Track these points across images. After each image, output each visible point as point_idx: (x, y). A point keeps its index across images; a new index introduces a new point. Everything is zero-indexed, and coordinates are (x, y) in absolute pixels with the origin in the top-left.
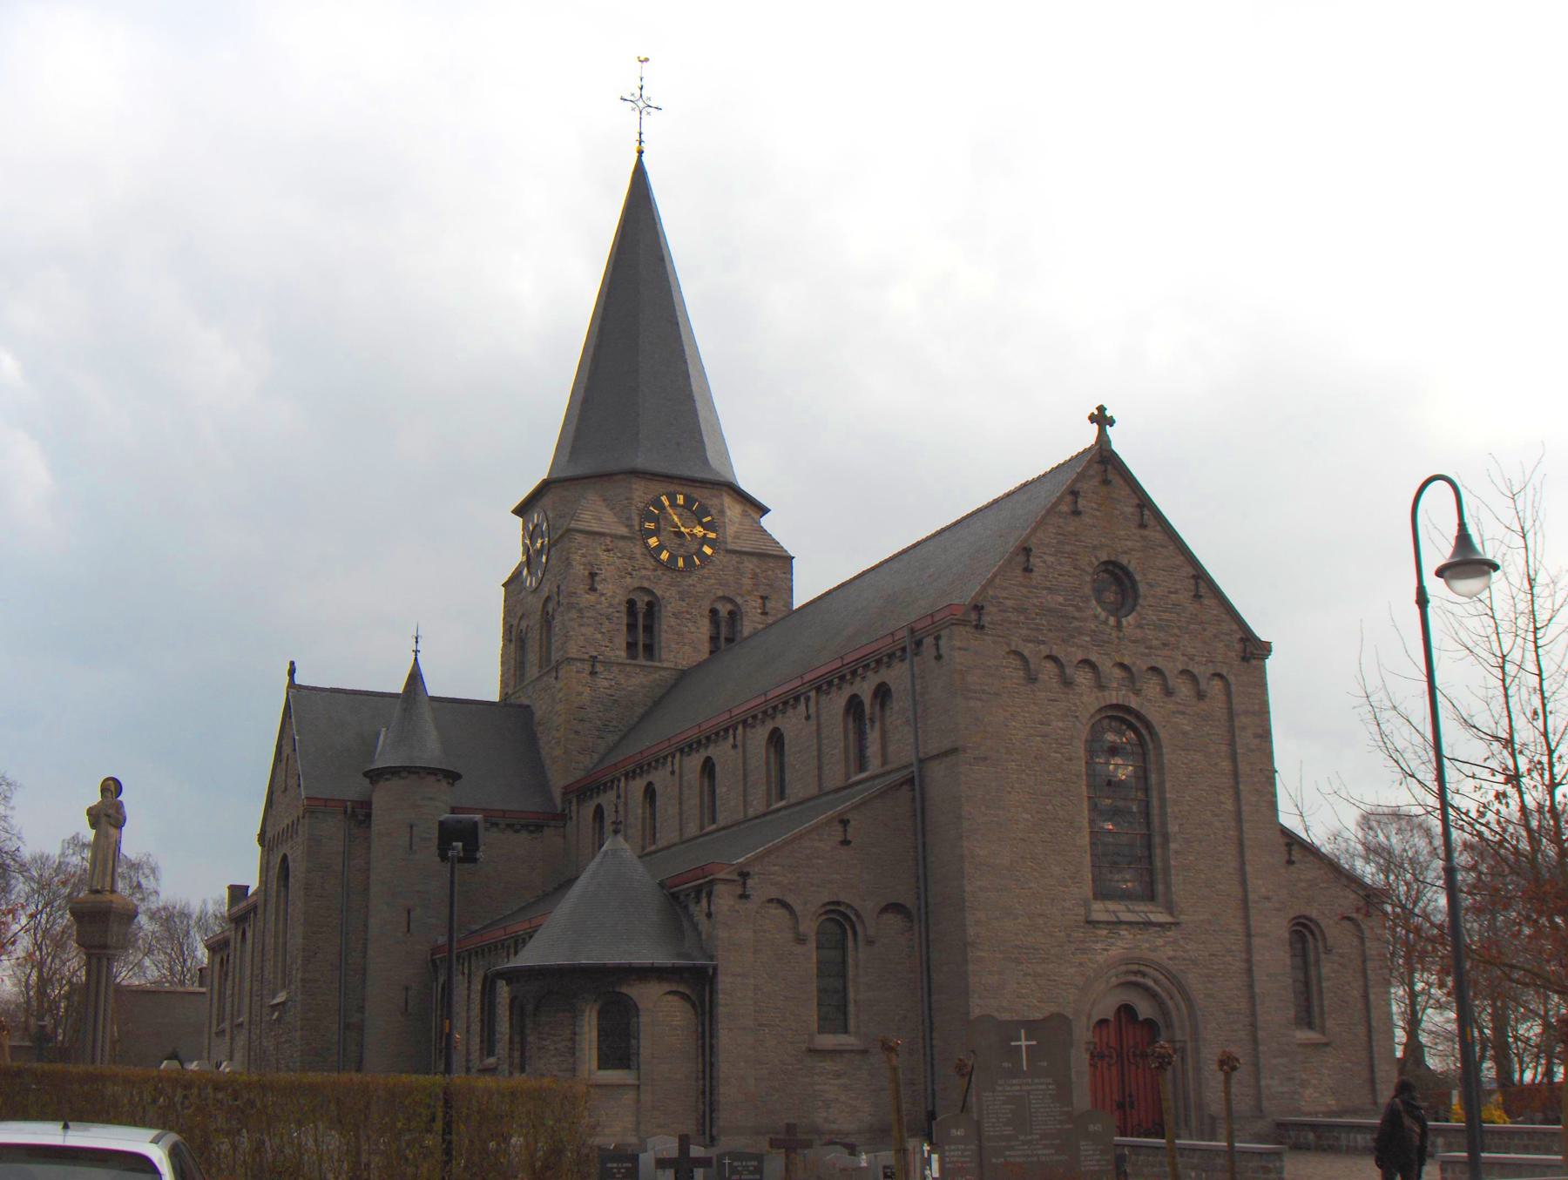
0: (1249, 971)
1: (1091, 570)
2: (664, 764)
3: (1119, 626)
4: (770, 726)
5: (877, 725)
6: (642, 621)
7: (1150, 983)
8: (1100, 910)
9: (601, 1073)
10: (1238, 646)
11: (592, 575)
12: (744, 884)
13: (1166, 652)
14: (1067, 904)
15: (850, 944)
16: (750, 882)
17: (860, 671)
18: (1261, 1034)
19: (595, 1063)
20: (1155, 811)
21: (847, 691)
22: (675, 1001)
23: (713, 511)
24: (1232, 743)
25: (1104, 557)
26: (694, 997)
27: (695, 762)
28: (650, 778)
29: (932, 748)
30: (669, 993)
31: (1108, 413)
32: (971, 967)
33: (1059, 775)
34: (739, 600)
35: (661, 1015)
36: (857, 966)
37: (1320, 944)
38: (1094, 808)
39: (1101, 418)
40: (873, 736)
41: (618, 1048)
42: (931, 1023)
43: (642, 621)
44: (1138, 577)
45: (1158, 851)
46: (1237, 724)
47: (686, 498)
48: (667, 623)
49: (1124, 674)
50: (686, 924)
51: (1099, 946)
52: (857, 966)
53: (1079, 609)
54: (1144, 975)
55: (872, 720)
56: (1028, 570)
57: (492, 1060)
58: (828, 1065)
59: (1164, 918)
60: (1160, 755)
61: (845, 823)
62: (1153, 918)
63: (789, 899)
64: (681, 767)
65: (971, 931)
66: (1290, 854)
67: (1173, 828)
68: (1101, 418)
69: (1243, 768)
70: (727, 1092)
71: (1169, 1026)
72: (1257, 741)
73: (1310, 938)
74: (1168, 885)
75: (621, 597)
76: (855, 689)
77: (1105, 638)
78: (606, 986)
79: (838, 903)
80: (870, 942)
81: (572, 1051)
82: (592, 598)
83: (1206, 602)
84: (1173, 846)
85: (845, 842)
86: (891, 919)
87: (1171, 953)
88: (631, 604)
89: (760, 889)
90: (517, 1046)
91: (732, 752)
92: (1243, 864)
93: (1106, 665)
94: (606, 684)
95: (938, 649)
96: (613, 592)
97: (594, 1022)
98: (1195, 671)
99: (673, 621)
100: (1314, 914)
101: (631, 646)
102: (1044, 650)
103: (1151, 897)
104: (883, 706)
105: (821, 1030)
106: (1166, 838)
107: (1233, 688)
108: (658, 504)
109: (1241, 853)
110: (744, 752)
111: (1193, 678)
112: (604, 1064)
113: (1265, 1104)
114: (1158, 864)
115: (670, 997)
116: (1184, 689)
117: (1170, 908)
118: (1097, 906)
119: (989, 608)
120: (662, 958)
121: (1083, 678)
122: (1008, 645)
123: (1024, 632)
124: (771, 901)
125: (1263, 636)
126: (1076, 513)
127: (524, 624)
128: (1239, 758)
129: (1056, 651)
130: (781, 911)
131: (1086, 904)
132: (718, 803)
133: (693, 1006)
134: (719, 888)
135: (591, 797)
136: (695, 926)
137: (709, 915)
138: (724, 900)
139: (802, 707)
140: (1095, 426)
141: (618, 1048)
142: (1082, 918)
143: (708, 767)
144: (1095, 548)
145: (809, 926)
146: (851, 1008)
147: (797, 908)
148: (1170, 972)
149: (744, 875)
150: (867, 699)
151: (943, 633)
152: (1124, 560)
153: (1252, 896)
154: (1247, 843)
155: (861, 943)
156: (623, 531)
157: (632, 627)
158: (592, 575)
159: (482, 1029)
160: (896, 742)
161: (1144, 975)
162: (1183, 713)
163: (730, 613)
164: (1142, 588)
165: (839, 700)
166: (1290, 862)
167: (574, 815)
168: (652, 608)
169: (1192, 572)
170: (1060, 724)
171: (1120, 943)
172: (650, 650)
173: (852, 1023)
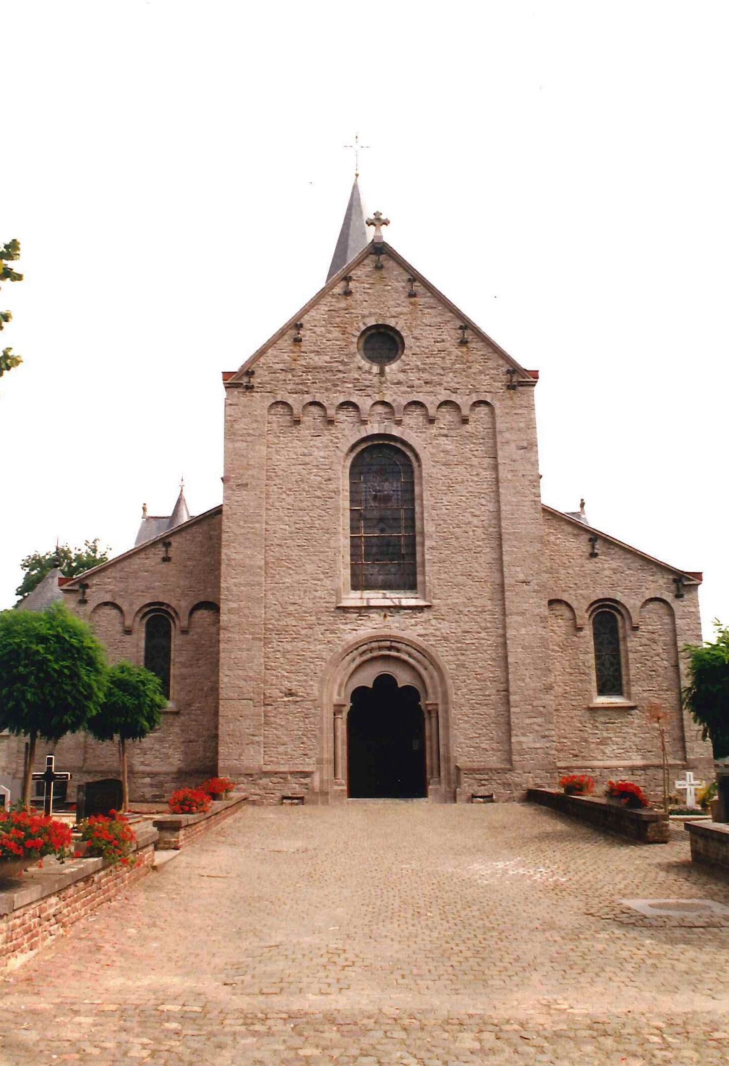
3: (382, 373)
7: (405, 657)
8: (353, 599)
12: (84, 593)
13: (428, 388)
18: (512, 698)
31: (383, 217)
32: (222, 646)
37: (627, 623)
44: (403, 334)
49: (387, 410)
56: (297, 341)
59: (421, 603)
61: (167, 545)
62: (404, 603)
63: (118, 602)
66: (593, 547)
67: (429, 528)
69: (503, 474)
73: (619, 617)
77: (367, 383)
85: (166, 559)
87: (423, 632)
98: (458, 401)
100: (618, 597)
102: (308, 398)
103: (411, 586)
113: (515, 758)
119: (259, 372)
123: (289, 387)
125: (526, 363)
130: (115, 612)
147: (125, 608)
152: (392, 323)
154: (504, 537)
162: (446, 436)
169: (459, 323)
171: (369, 624)
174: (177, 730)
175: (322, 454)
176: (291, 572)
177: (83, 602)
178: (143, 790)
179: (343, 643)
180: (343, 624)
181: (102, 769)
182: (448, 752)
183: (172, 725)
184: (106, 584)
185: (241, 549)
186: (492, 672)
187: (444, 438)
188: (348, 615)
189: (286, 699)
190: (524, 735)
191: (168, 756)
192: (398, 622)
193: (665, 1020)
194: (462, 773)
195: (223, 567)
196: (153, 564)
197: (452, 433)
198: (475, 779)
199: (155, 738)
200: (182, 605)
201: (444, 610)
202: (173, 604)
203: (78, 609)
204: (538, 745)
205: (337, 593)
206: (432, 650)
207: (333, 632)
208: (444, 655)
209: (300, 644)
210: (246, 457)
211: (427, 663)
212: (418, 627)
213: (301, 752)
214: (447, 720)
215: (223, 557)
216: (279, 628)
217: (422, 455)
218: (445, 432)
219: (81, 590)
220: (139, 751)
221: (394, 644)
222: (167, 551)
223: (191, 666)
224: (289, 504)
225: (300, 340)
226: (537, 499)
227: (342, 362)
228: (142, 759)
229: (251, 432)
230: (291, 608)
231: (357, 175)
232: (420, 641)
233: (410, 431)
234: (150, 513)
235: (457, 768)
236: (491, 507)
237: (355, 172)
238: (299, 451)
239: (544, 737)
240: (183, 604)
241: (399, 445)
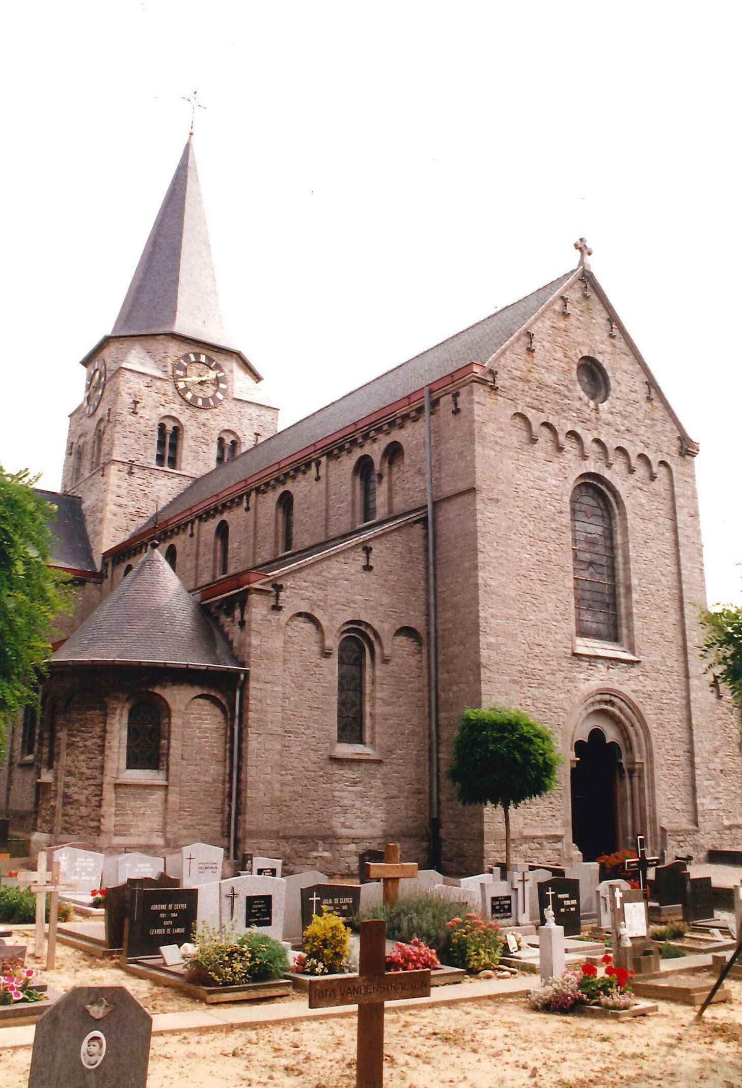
0: (688, 706)
1: (577, 361)
2: (184, 530)
4: (280, 490)
5: (385, 479)
6: (169, 443)
9: (130, 771)
10: (678, 443)
11: (136, 403)
12: (277, 597)
14: (558, 637)
15: (368, 660)
16: (282, 594)
17: (372, 434)
18: (697, 760)
19: (123, 762)
20: (620, 566)
21: (358, 453)
22: (205, 704)
23: (226, 370)
24: (674, 519)
25: (585, 354)
26: (224, 702)
27: (211, 525)
28: (172, 542)
29: (448, 489)
33: (553, 525)
34: (239, 434)
35: (193, 722)
36: (373, 682)
39: (581, 247)
41: (148, 749)
42: (438, 736)
43: (169, 443)
44: (609, 374)
45: (622, 600)
46: (677, 504)
47: (207, 358)
48: (187, 445)
49: (600, 450)
50: (217, 634)
51: (582, 676)
52: (373, 682)
53: (569, 390)
54: (612, 704)
55: (380, 476)
56: (530, 351)
57: (30, 758)
58: (348, 773)
60: (624, 519)
61: (368, 550)
63: (318, 614)
64: (199, 530)
65: (484, 653)
67: (634, 581)
68: (581, 247)
69: (682, 539)
70: (255, 794)
71: (630, 749)
74: (630, 630)
75: (155, 421)
76: (367, 450)
78: (139, 689)
79: (359, 622)
80: (386, 661)
81: (102, 749)
82: (132, 418)
83: (655, 404)
84: (635, 596)
85: (368, 568)
86: (402, 640)
87: (635, 688)
88: (162, 427)
89: (292, 601)
90: (46, 742)
91: (245, 514)
92: (683, 616)
93: (587, 438)
94: (140, 481)
95: (456, 404)
96: (151, 416)
97: (125, 720)
99: (192, 443)
101: (160, 459)
103: (615, 638)
104: (391, 463)
105: (341, 740)
106: (629, 589)
107: (675, 475)
108: (186, 358)
109: (681, 608)
110: (256, 513)
111: (648, 463)
112: (133, 762)
113: (700, 819)
114: (623, 611)
115: (201, 701)
116: (641, 471)
117: (632, 649)
118: (579, 641)
120: (197, 661)
121: (569, 446)
122: (516, 407)
123: (528, 400)
124: (300, 614)
126: (566, 315)
127: (82, 441)
128: (679, 531)
129: (552, 420)
130: (309, 627)
132: (230, 556)
133: (223, 710)
134: (254, 598)
135: (123, 561)
136: (225, 636)
137: (242, 624)
138: (258, 609)
139: (313, 471)
140: (578, 252)
141: (148, 749)
142: (570, 651)
143: (223, 531)
144: (579, 344)
145: (333, 642)
146: (368, 722)
147: (324, 623)
148: (632, 703)
149: (279, 588)
150: (377, 459)
151: (461, 391)
152: (600, 358)
153: (689, 644)
155: (378, 660)
156: (159, 374)
157: (161, 444)
158: (136, 403)
159: (25, 731)
160: (407, 487)
161: (612, 704)
163: (232, 442)
164: (613, 384)
165: (348, 462)
167: (109, 574)
168: (177, 432)
170: (554, 482)
172: (173, 462)
173: (367, 734)
174: (378, 783)
175: (554, 482)
176: (536, 609)
177: (277, 608)
178: (348, 860)
179: (579, 694)
180: (577, 672)
181: (300, 833)
182: (654, 813)
183: (374, 777)
184: (301, 589)
185: (496, 575)
186: (680, 734)
187: (639, 491)
188: (581, 663)
190: (704, 797)
191: (369, 816)
192: (619, 676)
194: (668, 833)
195: (481, 593)
196: (353, 571)
198: (676, 841)
199: (356, 793)
200: (385, 628)
201: (648, 667)
202: (376, 625)
203: (269, 617)
204: (713, 807)
206: (640, 706)
207: (571, 680)
208: (649, 713)
209: (546, 691)
210: (495, 468)
211: (635, 720)
212: (632, 682)
213: (550, 813)
214: (652, 781)
215: (480, 581)
216: (529, 671)
217: (627, 503)
218: (640, 485)
219: (274, 593)
220: (339, 809)
221: (613, 698)
222: (368, 558)
223: (392, 704)
224: (530, 531)
225: (533, 351)
227: (566, 386)
228: (342, 820)
229: (498, 440)
230: (537, 650)
231: (191, 134)
232: (633, 697)
233: (615, 476)
235: (663, 829)
236: (673, 569)
237: (190, 130)
238: (537, 473)
239: (717, 798)
240: (386, 626)
241: (603, 488)
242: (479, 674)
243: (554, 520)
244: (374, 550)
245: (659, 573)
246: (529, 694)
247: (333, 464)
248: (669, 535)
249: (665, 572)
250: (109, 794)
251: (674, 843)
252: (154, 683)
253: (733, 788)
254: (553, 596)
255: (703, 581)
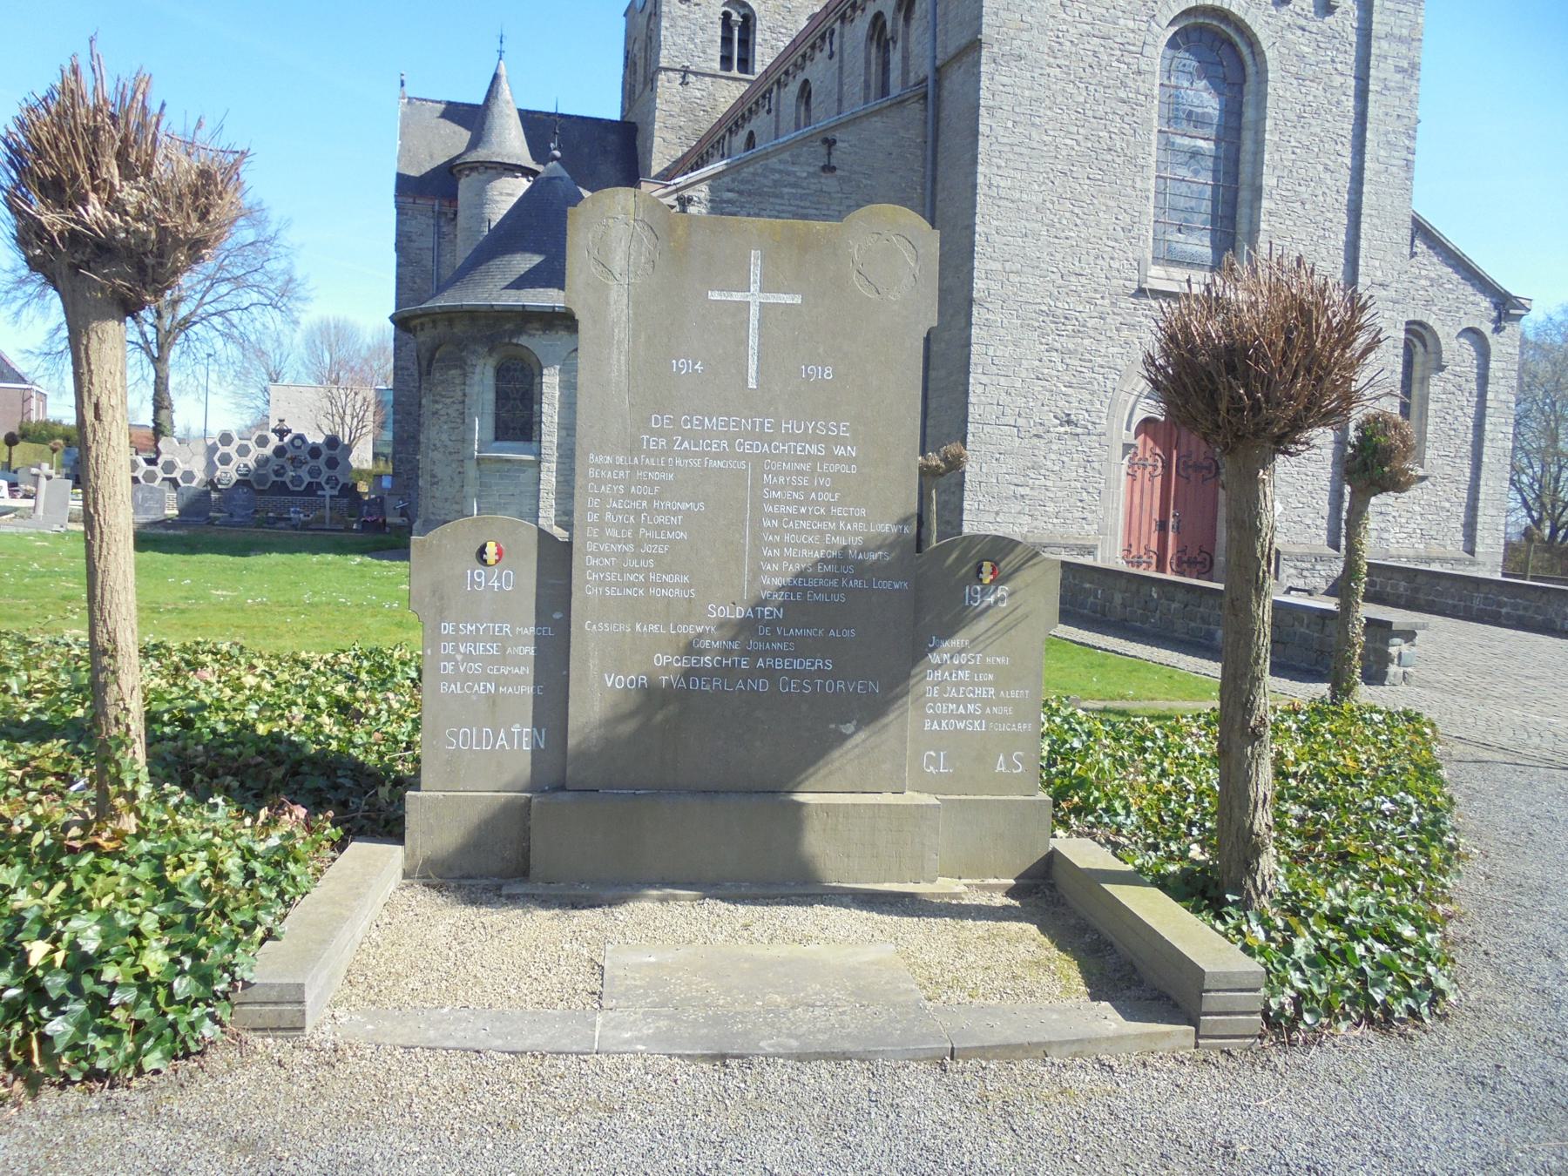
5: (899, 45)
30: (1276, 578)
38: (1168, 146)
40: (895, 57)
61: (830, 143)
67: (1268, 180)
72: (1399, 77)
85: (828, 168)
99: (768, 35)
100: (1432, 321)
101: (726, 61)
106: (1257, 191)
110: (777, 116)
118: (1155, 271)
128: (1371, 97)
131: (1140, 265)
157: (726, 41)
166: (1413, 255)
170: (1131, 24)
176: (1079, 222)
189: (1062, 429)
193: (252, 994)
197: (1312, 26)
198: (1296, 567)
205: (1140, 265)
209: (1087, 342)
218: (1303, 22)
226: (1410, 157)
234: (410, 91)
235: (1278, 552)
242: (970, 315)
243: (1124, 85)
244: (839, 144)
245: (1321, 168)
246: (1057, 345)
247: (848, 27)
248: (1350, 104)
249: (1332, 166)
250: (471, 471)
251: (1293, 571)
252: (519, 331)
253: (1447, 505)
254: (1112, 203)
255: (1411, 179)
